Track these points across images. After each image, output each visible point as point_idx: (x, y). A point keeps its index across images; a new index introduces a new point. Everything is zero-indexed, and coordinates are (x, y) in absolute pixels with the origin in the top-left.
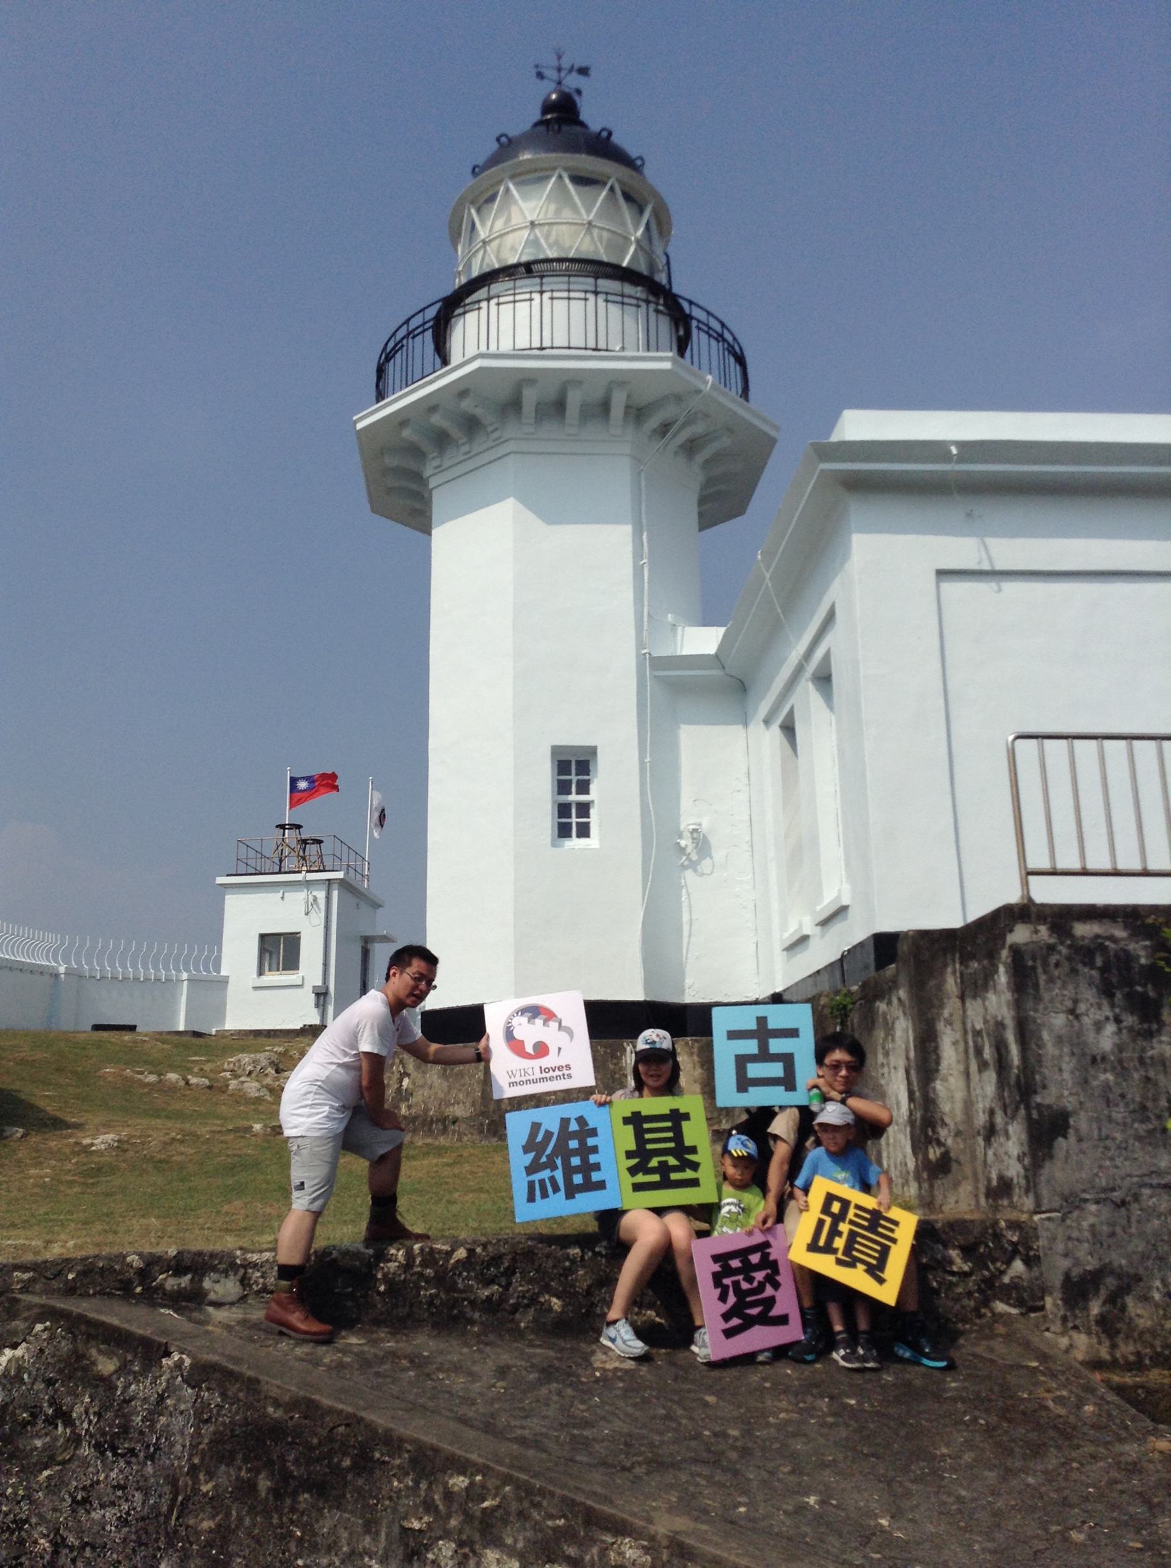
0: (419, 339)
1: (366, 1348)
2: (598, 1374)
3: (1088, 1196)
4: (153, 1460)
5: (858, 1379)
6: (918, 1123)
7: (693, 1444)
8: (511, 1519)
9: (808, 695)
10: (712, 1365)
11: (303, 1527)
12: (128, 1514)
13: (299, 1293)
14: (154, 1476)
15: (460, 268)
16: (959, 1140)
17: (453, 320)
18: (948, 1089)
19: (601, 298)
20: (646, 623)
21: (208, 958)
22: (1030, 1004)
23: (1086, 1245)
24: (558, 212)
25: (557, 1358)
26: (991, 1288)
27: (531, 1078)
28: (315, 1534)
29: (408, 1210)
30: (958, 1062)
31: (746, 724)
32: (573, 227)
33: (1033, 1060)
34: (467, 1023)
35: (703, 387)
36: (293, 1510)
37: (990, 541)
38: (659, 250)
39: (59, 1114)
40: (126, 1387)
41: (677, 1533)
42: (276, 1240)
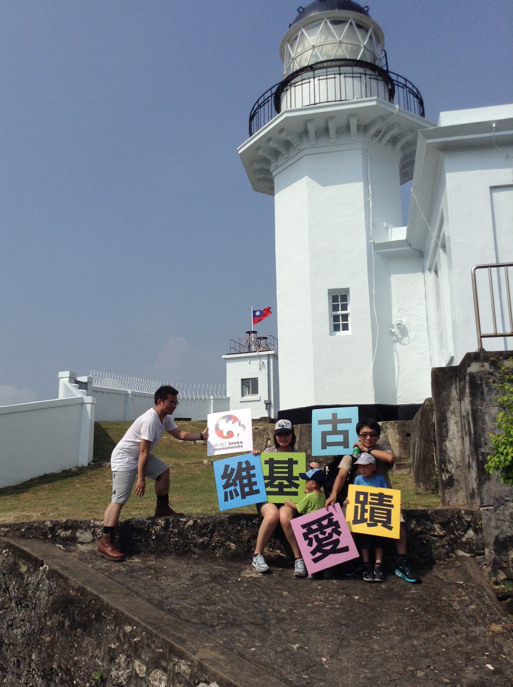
3: (508, 498)
16: (458, 470)
19: (368, 76)
20: (371, 228)
22: (479, 403)
24: (326, 39)
26: (455, 543)
28: (81, 647)
31: (424, 272)
32: (333, 45)
35: (394, 111)
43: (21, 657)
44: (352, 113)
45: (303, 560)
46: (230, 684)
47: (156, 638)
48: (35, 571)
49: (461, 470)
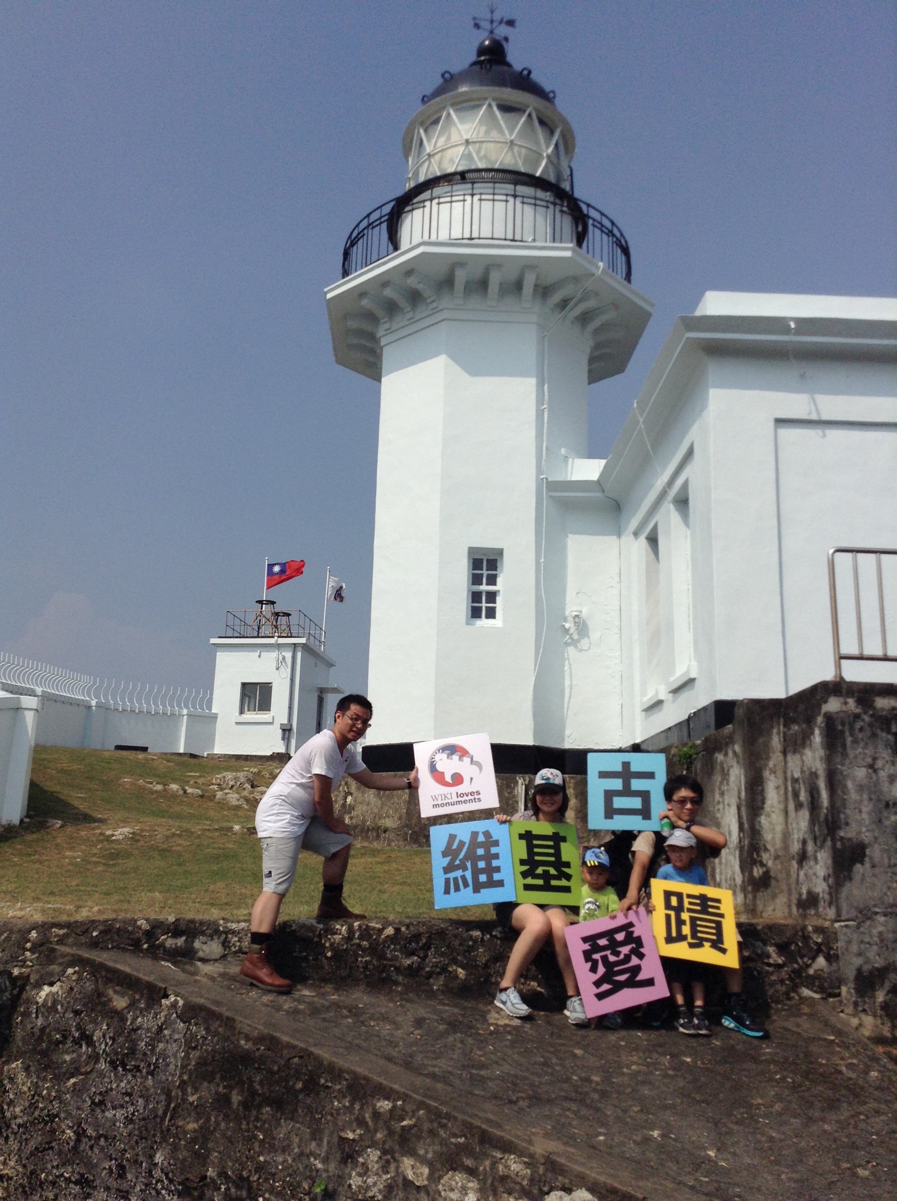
12: (133, 1114)
16: (777, 862)
19: (518, 200)
20: (544, 455)
22: (838, 759)
24: (487, 132)
26: (799, 978)
28: (274, 1139)
30: (779, 802)
31: (619, 535)
32: (499, 145)
35: (594, 270)
36: (257, 1119)
38: (564, 164)
43: (128, 1160)
44: (529, 265)
45: (581, 999)
46: (614, 1191)
47: (449, 1120)
48: (149, 1007)
49: (782, 863)
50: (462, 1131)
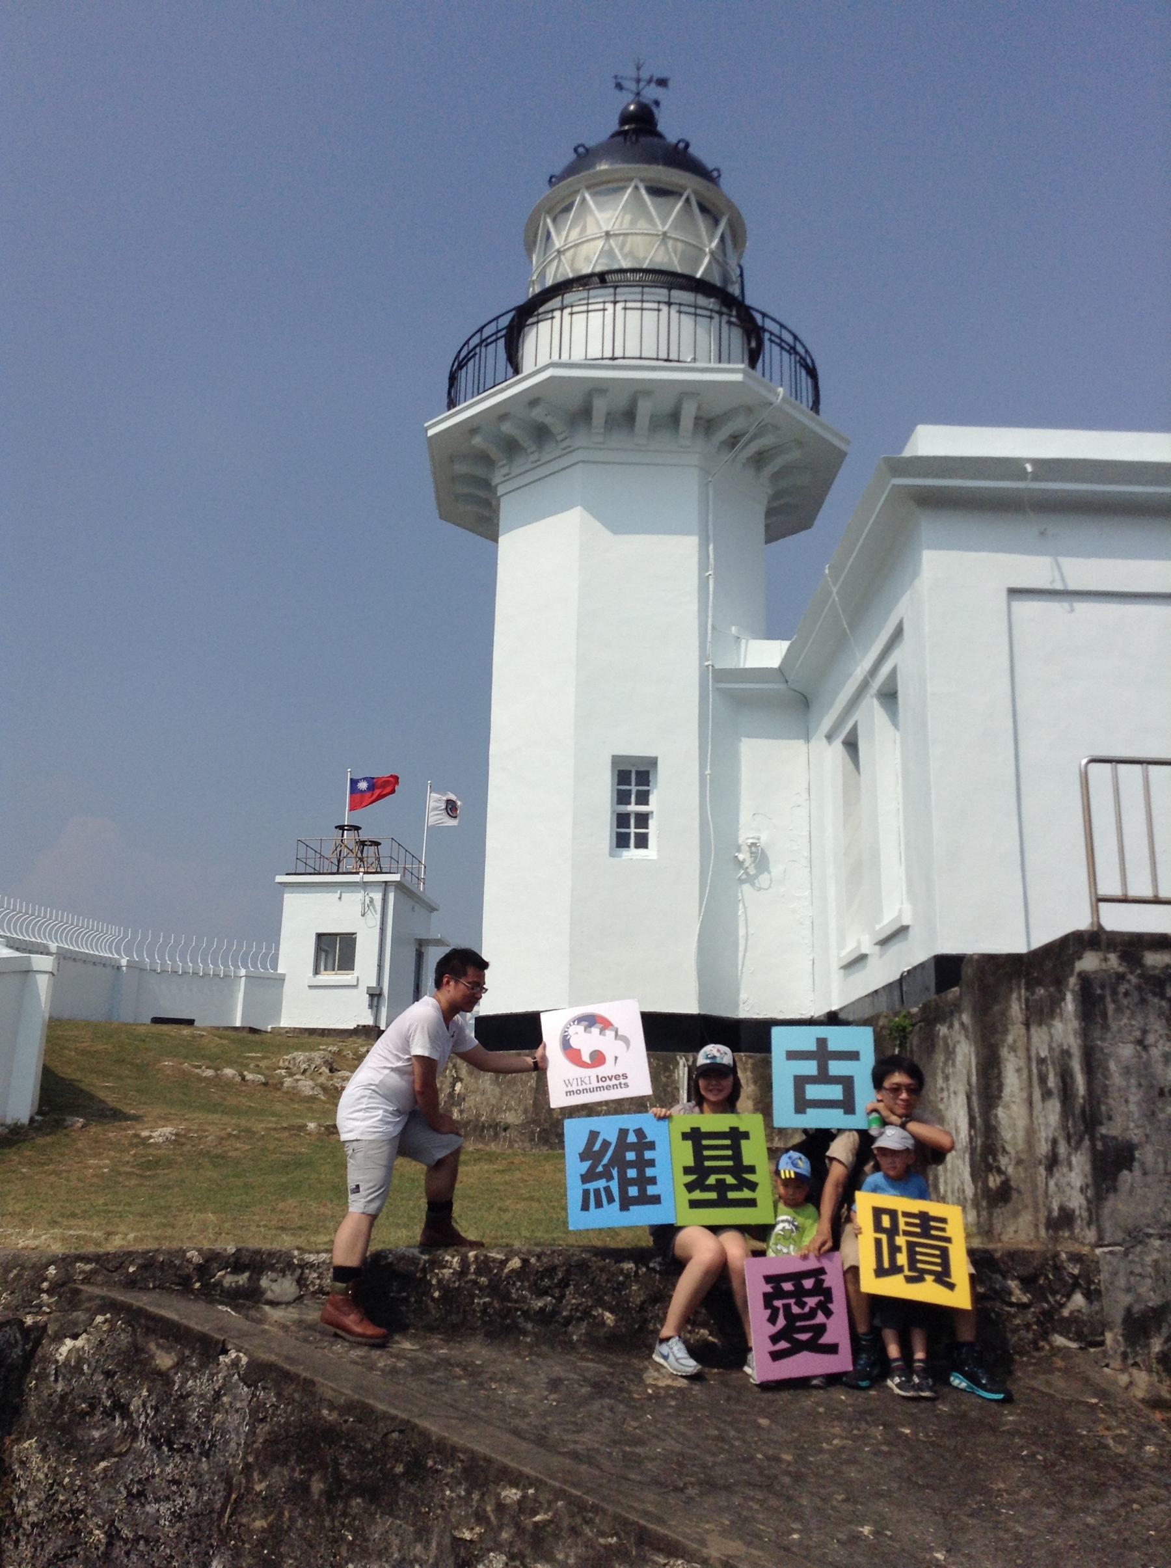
0: (492, 347)
1: (419, 1354)
2: (650, 1391)
3: (1151, 1231)
4: (207, 1457)
5: (913, 1408)
6: (978, 1150)
7: (747, 1467)
8: (563, 1534)
9: (872, 712)
10: (765, 1386)
11: (355, 1532)
12: (182, 1509)
13: (354, 1296)
14: (209, 1472)
15: (534, 278)
16: (1020, 1169)
17: (526, 329)
18: (1011, 1117)
19: (674, 309)
21: (266, 954)
22: (1097, 1033)
23: (1149, 1281)
24: (633, 223)
25: (610, 1374)
26: (1050, 1321)
27: (588, 1087)
28: (366, 1540)
29: (460, 1216)
31: (807, 739)
32: (648, 238)
33: (1099, 1091)
34: (522, 1031)
35: (771, 398)
36: (345, 1514)
37: (1061, 559)
38: (733, 262)
39: (119, 1106)
40: (184, 1382)
41: (730, 1557)
42: (332, 1242)
44: (688, 391)
48: (203, 1365)
50: (614, 1528)
